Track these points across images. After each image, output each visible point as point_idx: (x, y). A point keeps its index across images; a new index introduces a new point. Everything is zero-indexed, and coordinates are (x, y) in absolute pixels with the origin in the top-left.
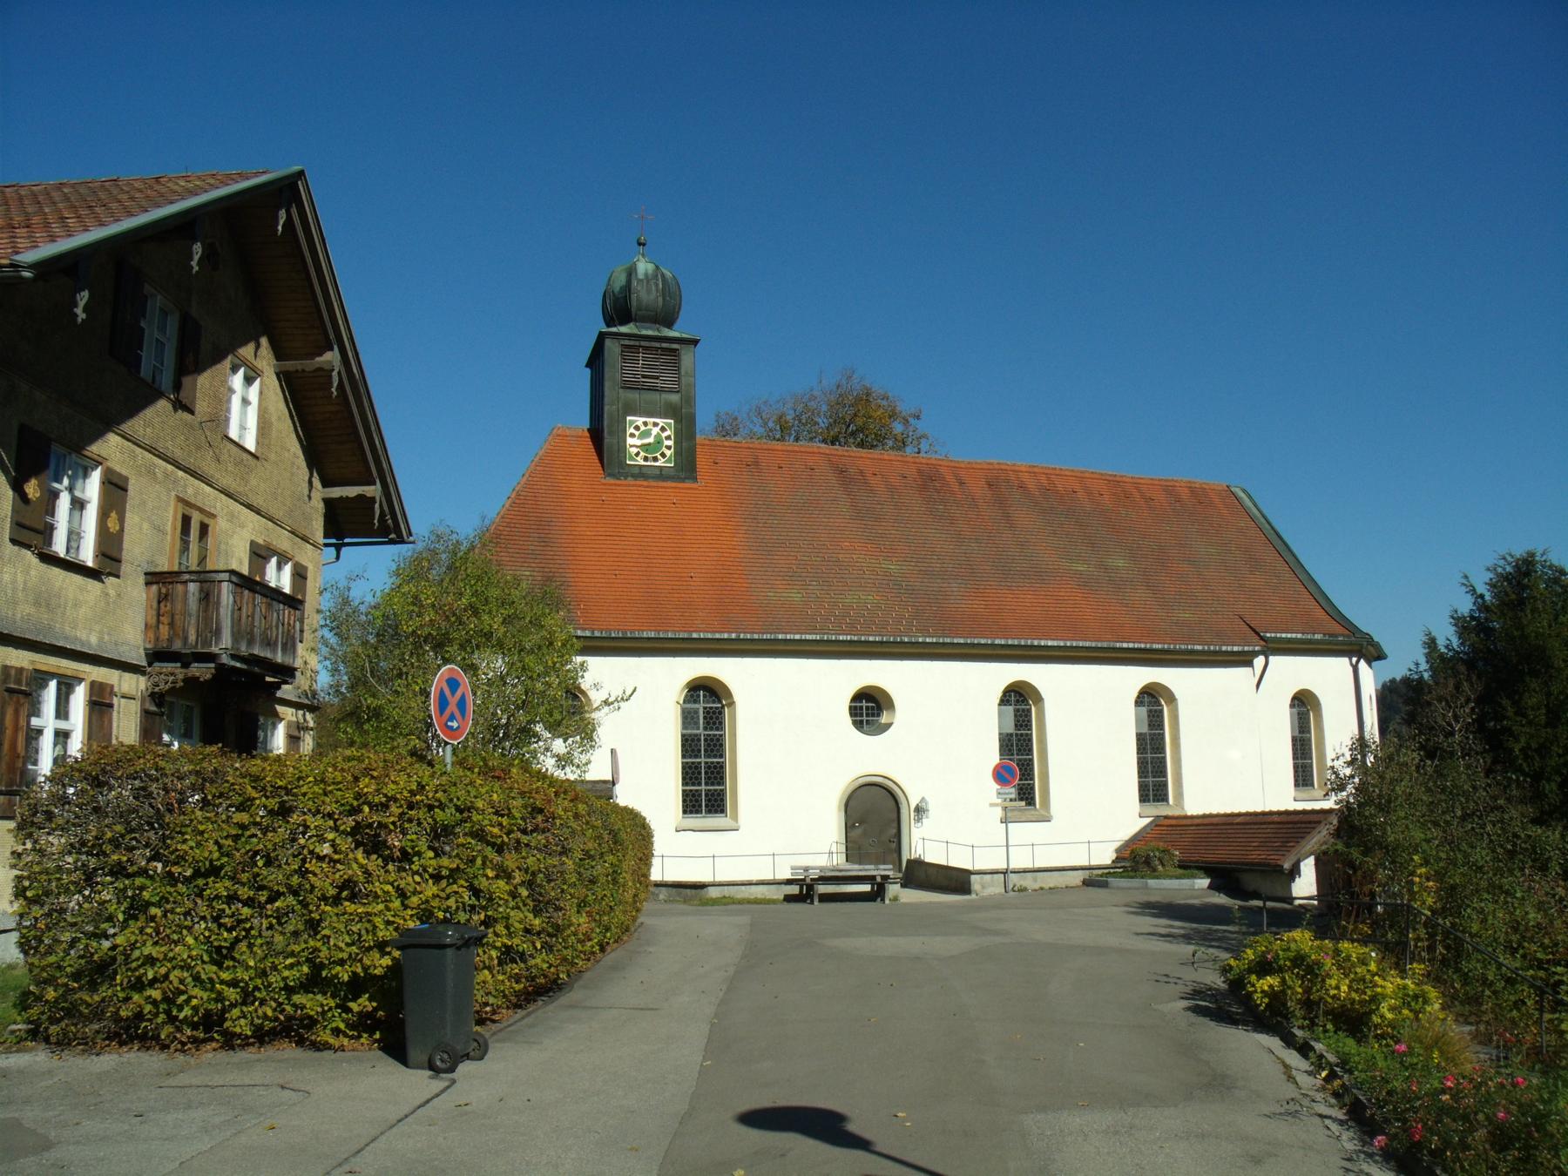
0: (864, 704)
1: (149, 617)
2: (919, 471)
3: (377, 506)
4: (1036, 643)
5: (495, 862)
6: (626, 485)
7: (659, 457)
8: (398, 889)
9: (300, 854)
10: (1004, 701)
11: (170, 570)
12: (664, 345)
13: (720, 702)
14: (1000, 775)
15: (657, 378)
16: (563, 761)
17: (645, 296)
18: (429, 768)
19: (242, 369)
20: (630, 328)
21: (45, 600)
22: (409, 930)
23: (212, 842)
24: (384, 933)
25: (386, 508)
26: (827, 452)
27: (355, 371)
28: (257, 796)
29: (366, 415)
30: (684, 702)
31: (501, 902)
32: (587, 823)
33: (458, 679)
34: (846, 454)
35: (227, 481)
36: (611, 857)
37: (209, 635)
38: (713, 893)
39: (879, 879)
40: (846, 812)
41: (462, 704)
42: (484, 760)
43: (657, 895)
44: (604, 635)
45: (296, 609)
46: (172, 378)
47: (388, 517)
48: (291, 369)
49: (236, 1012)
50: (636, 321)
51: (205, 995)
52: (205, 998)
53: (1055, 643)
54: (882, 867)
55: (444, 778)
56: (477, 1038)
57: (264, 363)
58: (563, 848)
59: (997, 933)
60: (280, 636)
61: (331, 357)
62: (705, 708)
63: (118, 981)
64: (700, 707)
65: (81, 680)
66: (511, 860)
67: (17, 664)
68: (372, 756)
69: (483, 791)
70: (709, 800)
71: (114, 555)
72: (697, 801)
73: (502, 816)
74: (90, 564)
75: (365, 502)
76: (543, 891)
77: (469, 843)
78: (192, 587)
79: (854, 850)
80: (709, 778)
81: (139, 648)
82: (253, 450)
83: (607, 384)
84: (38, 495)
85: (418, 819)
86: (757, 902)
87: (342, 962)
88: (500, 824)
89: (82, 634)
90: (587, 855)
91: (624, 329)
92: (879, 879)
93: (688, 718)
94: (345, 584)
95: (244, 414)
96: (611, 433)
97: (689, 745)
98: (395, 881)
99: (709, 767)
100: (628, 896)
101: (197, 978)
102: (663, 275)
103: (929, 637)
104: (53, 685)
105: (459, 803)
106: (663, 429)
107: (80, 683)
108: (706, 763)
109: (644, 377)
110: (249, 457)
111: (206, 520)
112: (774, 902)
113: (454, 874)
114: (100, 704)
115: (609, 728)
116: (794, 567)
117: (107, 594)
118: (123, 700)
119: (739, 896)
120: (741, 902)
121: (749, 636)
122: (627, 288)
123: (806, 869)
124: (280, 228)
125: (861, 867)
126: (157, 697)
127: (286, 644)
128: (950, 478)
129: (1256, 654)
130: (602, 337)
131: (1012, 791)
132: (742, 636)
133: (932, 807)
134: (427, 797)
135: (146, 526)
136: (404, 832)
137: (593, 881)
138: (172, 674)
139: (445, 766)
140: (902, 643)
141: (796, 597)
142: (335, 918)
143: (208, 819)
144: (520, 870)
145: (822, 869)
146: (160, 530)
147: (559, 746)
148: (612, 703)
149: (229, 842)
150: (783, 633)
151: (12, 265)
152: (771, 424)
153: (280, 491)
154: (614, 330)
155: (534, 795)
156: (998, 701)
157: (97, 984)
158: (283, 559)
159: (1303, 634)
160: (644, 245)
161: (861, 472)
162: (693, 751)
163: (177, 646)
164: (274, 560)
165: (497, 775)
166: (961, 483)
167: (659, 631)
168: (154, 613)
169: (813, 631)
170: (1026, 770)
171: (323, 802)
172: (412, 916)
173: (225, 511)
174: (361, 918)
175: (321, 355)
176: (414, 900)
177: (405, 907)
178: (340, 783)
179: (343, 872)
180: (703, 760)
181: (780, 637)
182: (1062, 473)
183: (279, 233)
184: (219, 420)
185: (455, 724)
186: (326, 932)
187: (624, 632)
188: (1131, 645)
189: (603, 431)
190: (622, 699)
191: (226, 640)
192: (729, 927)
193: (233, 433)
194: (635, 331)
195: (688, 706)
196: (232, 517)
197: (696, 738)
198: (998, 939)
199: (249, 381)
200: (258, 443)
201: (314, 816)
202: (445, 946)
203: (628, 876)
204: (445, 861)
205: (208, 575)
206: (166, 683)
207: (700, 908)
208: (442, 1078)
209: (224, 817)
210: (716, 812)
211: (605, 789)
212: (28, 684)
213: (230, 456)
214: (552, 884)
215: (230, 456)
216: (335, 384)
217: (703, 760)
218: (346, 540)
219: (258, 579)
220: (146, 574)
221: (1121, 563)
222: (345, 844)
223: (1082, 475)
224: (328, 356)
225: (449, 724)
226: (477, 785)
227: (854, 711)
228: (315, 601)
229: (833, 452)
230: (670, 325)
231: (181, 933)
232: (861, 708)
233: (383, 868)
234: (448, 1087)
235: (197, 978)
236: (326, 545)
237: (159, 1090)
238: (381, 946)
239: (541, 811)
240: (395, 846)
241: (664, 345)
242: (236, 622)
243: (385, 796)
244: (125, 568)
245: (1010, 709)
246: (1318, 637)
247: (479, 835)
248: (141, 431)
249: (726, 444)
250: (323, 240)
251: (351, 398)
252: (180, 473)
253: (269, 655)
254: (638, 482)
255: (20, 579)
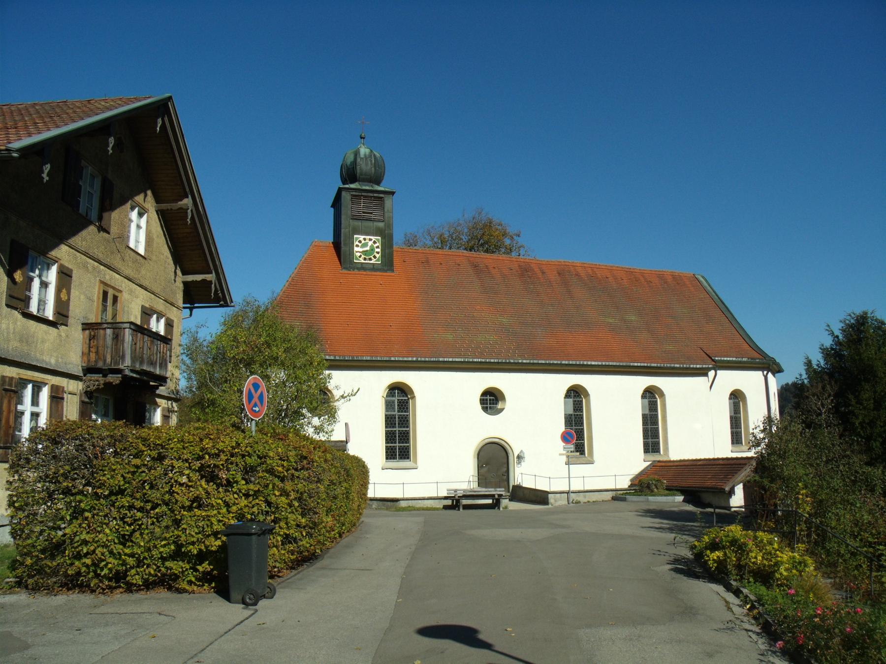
0: (488, 397)
1: (84, 349)
2: (519, 266)
3: (213, 285)
4: (585, 363)
5: (280, 487)
6: (354, 274)
7: (373, 258)
8: (225, 502)
9: (169, 482)
10: (567, 396)
11: (96, 322)
12: (375, 195)
13: (407, 396)
14: (565, 438)
15: (371, 213)
16: (318, 429)
17: (364, 167)
18: (242, 434)
19: (137, 209)
20: (356, 185)
21: (25, 339)
22: (231, 525)
23: (120, 475)
24: (217, 527)
25: (218, 287)
26: (468, 255)
27: (201, 209)
28: (145, 449)
29: (207, 234)
30: (387, 396)
31: (283, 509)
32: (332, 465)
33: (259, 383)
34: (478, 256)
35: (128, 272)
36: (345, 484)
37: (118, 358)
38: (403, 504)
39: (496, 496)
40: (478, 458)
41: (261, 397)
42: (273, 429)
43: (371, 505)
44: (341, 358)
45: (167, 344)
46: (97, 213)
47: (219, 292)
48: (165, 208)
49: (133, 571)
50: (359, 181)
51: (116, 562)
52: (116, 563)
53: (596, 363)
54: (498, 489)
55: (251, 439)
56: (270, 586)
57: (149, 205)
58: (318, 479)
59: (563, 527)
60: (158, 359)
61: (187, 202)
62: (398, 400)
63: (67, 554)
64: (396, 399)
65: (46, 384)
66: (289, 486)
67: (10, 375)
68: (210, 427)
69: (273, 446)
70: (401, 452)
71: (65, 313)
72: (394, 452)
73: (284, 461)
74: (51, 318)
75: (206, 284)
76: (307, 503)
77: (265, 476)
78: (109, 331)
79: (482, 480)
80: (401, 439)
81: (78, 366)
82: (143, 254)
83: (343, 217)
84: (21, 279)
85: (236, 463)
86: (428, 509)
87: (193, 543)
88: (283, 465)
89: (46, 358)
90: (332, 483)
91: (352, 186)
92: (496, 496)
93: (389, 405)
94: (195, 330)
95: (138, 234)
96: (345, 245)
97: (389, 421)
98: (223, 497)
99: (401, 433)
100: (355, 506)
101: (111, 552)
102: (375, 156)
103: (525, 359)
104: (30, 387)
105: (259, 454)
106: (375, 242)
107: (45, 386)
108: (399, 431)
109: (364, 213)
110: (141, 258)
111: (117, 294)
112: (437, 509)
113: (257, 494)
114: (56, 398)
115: (344, 411)
116: (449, 320)
117: (60, 336)
118: (69, 395)
119: (418, 506)
120: (419, 509)
121: (423, 359)
122: (355, 162)
123: (456, 491)
124: (158, 129)
125: (487, 490)
126: (88, 394)
127: (162, 363)
128: (537, 270)
129: (710, 369)
130: (340, 190)
131: (572, 447)
132: (419, 359)
133: (527, 456)
134: (241, 450)
135: (82, 297)
136: (228, 470)
137: (335, 498)
138: (97, 381)
139: (252, 432)
140: (510, 363)
141: (450, 337)
142: (189, 518)
143: (118, 462)
144: (294, 491)
145: (464, 491)
146: (90, 299)
147: (316, 421)
148: (346, 397)
149: (130, 475)
150: (442, 357)
151: (7, 150)
152: (435, 240)
153: (158, 277)
154: (347, 186)
155: (302, 449)
156: (564, 396)
157: (55, 555)
158: (160, 316)
159: (736, 358)
160: (364, 138)
161: (487, 266)
162: (391, 424)
163: (100, 365)
164: (155, 316)
165: (281, 438)
166: (543, 273)
167: (372, 357)
168: (87, 346)
169: (460, 356)
170: (580, 435)
171: (183, 453)
172: (233, 517)
173: (127, 289)
174: (204, 518)
175: (181, 200)
176: (234, 508)
177: (229, 512)
178: (192, 442)
179: (194, 493)
180: (397, 429)
181: (441, 359)
182: (600, 267)
183: (158, 131)
184: (124, 237)
185: (257, 409)
186: (184, 526)
187: (353, 357)
188: (639, 364)
189: (340, 243)
190: (352, 395)
191: (128, 362)
192: (412, 524)
193: (132, 245)
194: (359, 187)
195: (389, 398)
196: (131, 292)
197: (393, 417)
198: (564, 530)
199: (140, 215)
200: (146, 250)
201: (177, 461)
202: (251, 534)
203: (355, 495)
204: (251, 486)
205: (118, 324)
206: (94, 386)
207: (396, 513)
208: (250, 609)
209: (126, 461)
210: (405, 458)
211: (342, 446)
212: (16, 386)
213: (130, 257)
214: (312, 499)
215: (130, 257)
216: (189, 217)
217: (397, 429)
218: (196, 305)
219: (146, 327)
220: (82, 324)
221: (633, 318)
222: (195, 476)
223: (611, 268)
224: (185, 201)
225: (254, 409)
226: (270, 443)
227: (483, 402)
228: (178, 339)
229: (471, 255)
230: (378, 183)
231: (102, 527)
232: (487, 400)
233: (216, 490)
234: (253, 614)
235: (111, 552)
236: (184, 308)
237: (90, 616)
238: (216, 534)
239: (306, 458)
240: (223, 478)
241: (375, 195)
242: (134, 351)
243: (218, 449)
244: (71, 321)
245: (571, 401)
246: (745, 359)
247: (271, 471)
248: (80, 244)
249: (410, 251)
250: (183, 135)
251: (198, 225)
252: (102, 267)
253: (152, 370)
254: (360, 272)
255: (11, 327)
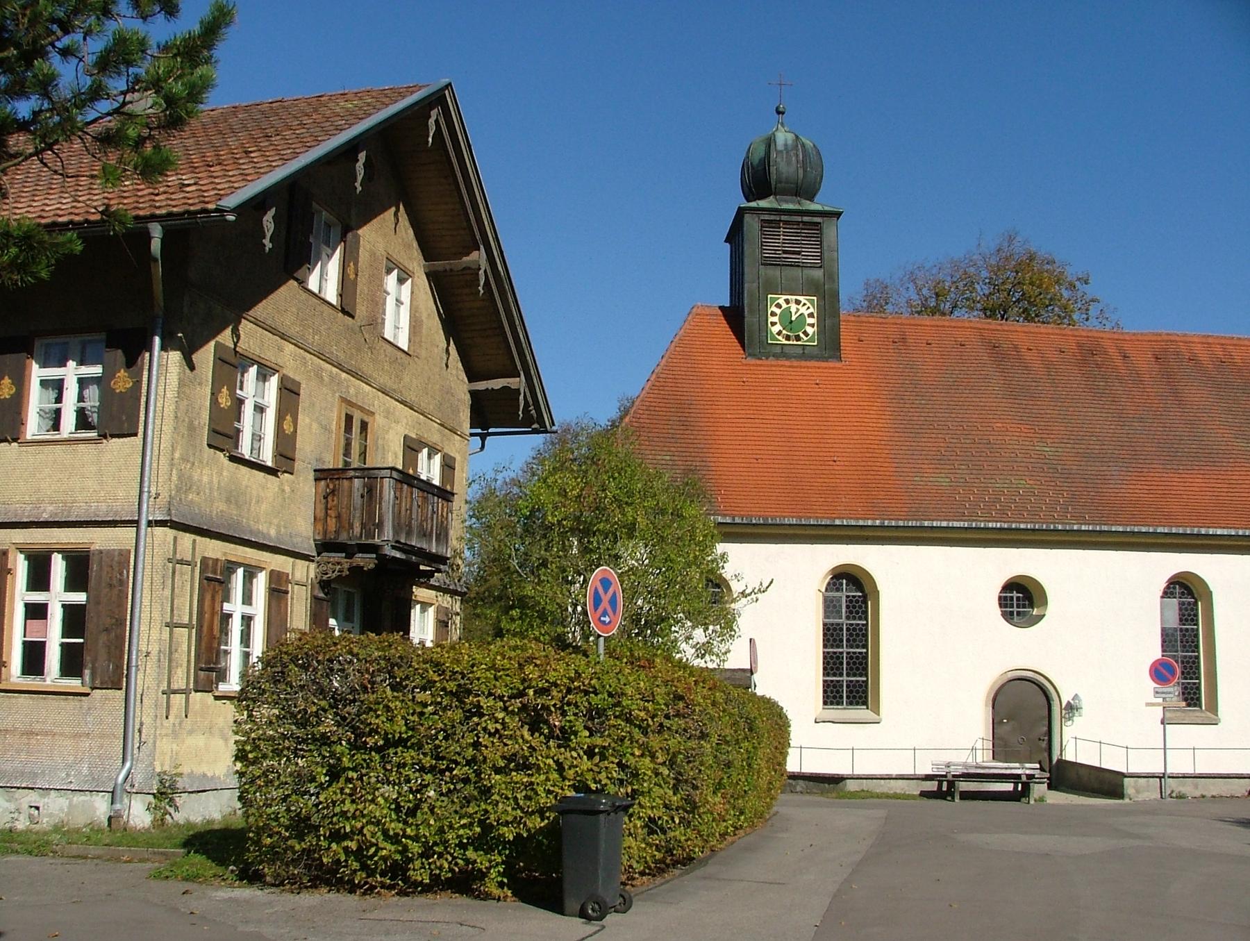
0: (1015, 594)
1: (318, 511)
2: (1079, 345)
3: (521, 397)
4: (1203, 531)
5: (641, 742)
6: (768, 366)
7: (802, 335)
8: (557, 762)
9: (474, 730)
10: (1167, 593)
11: (336, 467)
12: (806, 219)
14: (1159, 673)
15: (799, 253)
16: (704, 650)
17: (784, 168)
18: (584, 658)
19: (396, 271)
20: (769, 202)
21: (234, 496)
22: (566, 797)
23: (400, 718)
24: (544, 800)
25: (530, 399)
26: (979, 325)
27: (500, 268)
28: (437, 679)
29: (511, 311)
30: (826, 590)
31: (646, 778)
32: (724, 711)
33: (610, 578)
34: (999, 328)
35: (384, 380)
36: (747, 744)
37: (372, 528)
38: (851, 786)
39: (1024, 779)
40: (993, 708)
41: (613, 602)
42: (631, 650)
43: (795, 787)
44: (745, 521)
45: (449, 501)
46: (336, 288)
47: (532, 408)
48: (440, 269)
50: (775, 194)
51: (393, 848)
52: (393, 849)
53: (1225, 532)
54: (1028, 765)
55: (598, 667)
56: (623, 893)
57: (415, 264)
58: (701, 732)
59: (1138, 837)
60: (434, 528)
61: (478, 257)
62: (847, 597)
63: (322, 833)
65: (262, 569)
66: (655, 742)
67: (218, 555)
68: (533, 646)
69: (631, 679)
70: (851, 692)
71: (289, 455)
72: (838, 692)
73: (648, 701)
74: (269, 464)
75: (510, 395)
76: (682, 771)
77: (619, 725)
78: (357, 483)
79: (1001, 749)
80: (851, 669)
81: (309, 539)
82: (406, 349)
83: (747, 261)
84: (229, 404)
85: (576, 702)
86: (896, 796)
87: (507, 824)
88: (645, 709)
89: (263, 528)
90: (723, 740)
91: (763, 204)
92: (1024, 779)
93: (830, 606)
94: (493, 476)
95: (398, 313)
96: (751, 311)
97: (831, 635)
98: (555, 755)
99: (851, 658)
100: (763, 783)
101: (385, 833)
102: (803, 145)
103: (1085, 524)
104: (240, 571)
105: (611, 690)
107: (261, 571)
108: (848, 653)
109: (785, 252)
110: (403, 355)
111: (366, 418)
112: (913, 797)
114: (278, 591)
115: (748, 617)
116: (943, 450)
117: (283, 491)
118: (296, 587)
120: (879, 796)
122: (766, 160)
124: (430, 140)
125: (1006, 765)
126: (324, 585)
127: (440, 534)
128: (1112, 351)
130: (741, 212)
131: (1174, 690)
132: (886, 523)
133: (1085, 704)
134: (583, 683)
135: (315, 426)
136: (564, 714)
137: (729, 765)
138: (338, 563)
139: (598, 656)
140: (1055, 530)
141: (945, 482)
142: (503, 786)
143: (396, 698)
144: (662, 751)
145: (965, 765)
146: (326, 429)
147: (699, 635)
148: (750, 594)
149: (416, 718)
150: (929, 520)
151: (216, 210)
152: (925, 291)
153: (430, 386)
154: (753, 204)
155: (675, 683)
156: (1161, 594)
157: (305, 834)
158: (433, 451)
160: (783, 113)
161: (1016, 347)
162: (835, 640)
163: (343, 538)
164: (425, 451)
165: (642, 664)
167: (800, 518)
168: (323, 506)
169: (961, 517)
170: (1190, 668)
171: (494, 686)
172: (569, 786)
173: (382, 409)
174: (526, 786)
175: (468, 254)
177: (564, 779)
178: (508, 669)
179: (513, 747)
180: (845, 650)
181: (926, 524)
182: (1241, 343)
183: (430, 144)
184: (376, 323)
185: (607, 619)
186: (496, 797)
187: (766, 518)
189: (743, 309)
190: (759, 590)
191: (388, 533)
192: (863, 820)
193: (388, 335)
194: (775, 205)
196: (388, 414)
198: (1137, 842)
199: (401, 281)
200: (410, 341)
201: (487, 698)
203: (763, 764)
204: (598, 741)
205: (372, 471)
206: (333, 572)
207: (837, 800)
208: (594, 924)
209: (410, 697)
211: (744, 678)
212: (221, 574)
213: (386, 356)
214: (691, 765)
215: (386, 356)
216: (482, 283)
217: (845, 650)
218: (491, 430)
219: (411, 472)
220: (315, 471)
224: (474, 255)
225: (602, 619)
226: (626, 673)
227: (1003, 602)
228: (464, 491)
230: (811, 199)
231: (374, 794)
233: (545, 744)
234: (599, 931)
235: (385, 833)
236: (472, 435)
237: (360, 922)
238: (541, 812)
239: (681, 698)
240: (555, 726)
241: (806, 219)
242: (397, 516)
243: (547, 681)
244: (298, 465)
245: (1174, 602)
248: (311, 340)
249: (872, 320)
250: (470, 146)
252: (344, 375)
253: (425, 546)
254: (780, 363)
255: (215, 480)
